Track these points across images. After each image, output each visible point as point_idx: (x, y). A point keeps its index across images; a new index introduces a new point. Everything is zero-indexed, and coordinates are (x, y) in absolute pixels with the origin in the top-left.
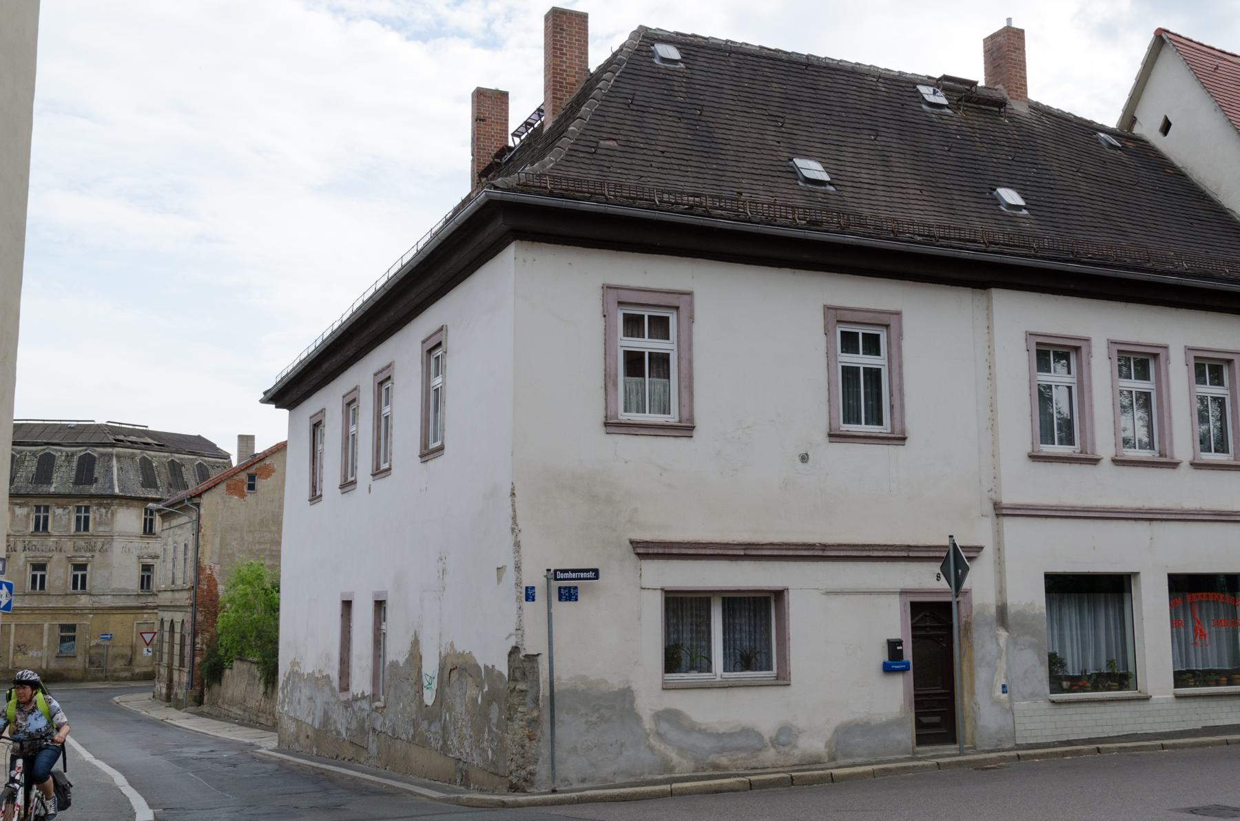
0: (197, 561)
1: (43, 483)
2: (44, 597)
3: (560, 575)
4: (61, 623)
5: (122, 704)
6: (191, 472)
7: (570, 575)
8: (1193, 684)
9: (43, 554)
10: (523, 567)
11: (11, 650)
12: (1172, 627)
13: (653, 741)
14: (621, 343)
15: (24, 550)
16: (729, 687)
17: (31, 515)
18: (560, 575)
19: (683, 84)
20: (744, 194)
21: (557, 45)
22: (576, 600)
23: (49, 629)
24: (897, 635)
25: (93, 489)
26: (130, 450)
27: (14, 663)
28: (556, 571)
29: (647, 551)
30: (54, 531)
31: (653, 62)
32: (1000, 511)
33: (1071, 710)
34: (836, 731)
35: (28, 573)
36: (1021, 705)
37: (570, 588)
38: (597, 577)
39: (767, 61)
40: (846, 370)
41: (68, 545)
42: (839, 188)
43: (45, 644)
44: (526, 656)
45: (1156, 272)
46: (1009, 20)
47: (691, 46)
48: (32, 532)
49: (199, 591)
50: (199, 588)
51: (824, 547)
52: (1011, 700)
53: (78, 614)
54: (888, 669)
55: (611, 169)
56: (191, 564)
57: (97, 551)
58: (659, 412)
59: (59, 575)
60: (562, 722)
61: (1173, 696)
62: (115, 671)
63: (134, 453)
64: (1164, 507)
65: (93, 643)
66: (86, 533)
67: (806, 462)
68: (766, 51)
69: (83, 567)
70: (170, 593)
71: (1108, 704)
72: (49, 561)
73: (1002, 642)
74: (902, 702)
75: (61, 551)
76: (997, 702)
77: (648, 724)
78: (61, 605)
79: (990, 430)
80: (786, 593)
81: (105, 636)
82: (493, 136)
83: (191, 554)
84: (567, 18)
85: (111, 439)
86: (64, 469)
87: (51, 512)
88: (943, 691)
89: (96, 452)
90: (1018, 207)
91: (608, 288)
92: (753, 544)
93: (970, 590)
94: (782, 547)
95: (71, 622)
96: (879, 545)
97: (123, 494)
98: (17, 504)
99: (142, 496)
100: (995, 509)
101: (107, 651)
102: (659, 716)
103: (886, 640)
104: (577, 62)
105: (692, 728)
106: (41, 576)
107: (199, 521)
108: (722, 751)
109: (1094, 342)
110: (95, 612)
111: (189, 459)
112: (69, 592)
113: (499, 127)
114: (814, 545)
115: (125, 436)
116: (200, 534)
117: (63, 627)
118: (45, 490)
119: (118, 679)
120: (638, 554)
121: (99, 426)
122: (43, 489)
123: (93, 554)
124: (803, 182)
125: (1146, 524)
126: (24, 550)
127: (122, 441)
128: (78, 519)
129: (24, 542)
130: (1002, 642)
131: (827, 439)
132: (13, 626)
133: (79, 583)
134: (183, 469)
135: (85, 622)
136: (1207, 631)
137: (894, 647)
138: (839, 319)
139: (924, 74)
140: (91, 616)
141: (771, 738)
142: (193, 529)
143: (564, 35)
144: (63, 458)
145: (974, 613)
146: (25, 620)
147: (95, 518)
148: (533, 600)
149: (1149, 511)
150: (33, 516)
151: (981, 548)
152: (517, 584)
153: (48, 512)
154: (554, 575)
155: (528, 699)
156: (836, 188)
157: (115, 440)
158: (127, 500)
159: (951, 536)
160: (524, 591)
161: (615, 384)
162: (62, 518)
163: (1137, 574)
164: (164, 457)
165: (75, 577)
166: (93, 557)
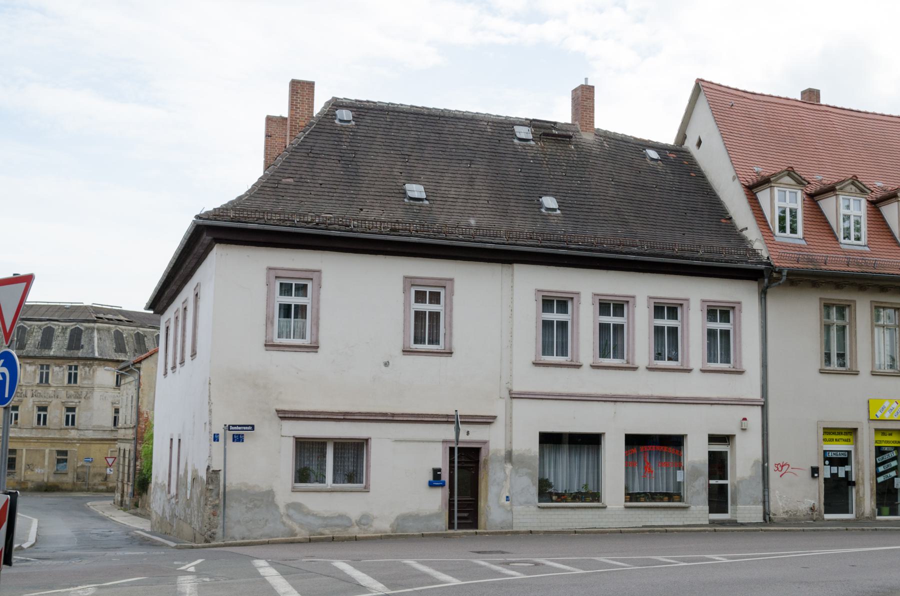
0: (138, 408)
1: (45, 348)
2: (45, 430)
3: (231, 428)
4: (57, 449)
5: (91, 507)
6: (152, 341)
7: (238, 428)
9: (45, 399)
10: (213, 423)
11: (23, 468)
12: (626, 466)
13: (285, 519)
14: (277, 299)
15: (32, 396)
17: (37, 371)
18: (231, 428)
19: (350, 136)
22: (243, 441)
23: (49, 454)
24: (438, 465)
25: (80, 353)
27: (25, 477)
28: (229, 426)
29: (285, 416)
31: (334, 123)
32: (514, 396)
33: (551, 512)
34: (397, 518)
36: (517, 508)
37: (239, 435)
38: (253, 429)
39: (413, 116)
41: (63, 393)
42: (432, 202)
43: (46, 463)
44: (213, 471)
45: (621, 253)
46: (586, 79)
47: (361, 109)
49: (139, 429)
50: (139, 427)
51: (393, 415)
52: (511, 505)
53: (69, 443)
54: (431, 485)
55: (309, 193)
56: (134, 410)
57: (83, 399)
58: (300, 338)
59: (56, 415)
60: (232, 507)
62: (94, 485)
65: (80, 464)
66: (75, 385)
68: (415, 108)
70: (124, 430)
71: (577, 510)
72: (49, 405)
73: (508, 471)
75: (57, 397)
76: (502, 506)
77: (282, 510)
78: (58, 437)
80: (369, 440)
82: (276, 146)
83: (134, 403)
84: (301, 86)
85: (94, 317)
86: (60, 338)
87: (51, 370)
88: (471, 499)
90: (554, 210)
92: (348, 413)
93: (489, 441)
95: (64, 449)
96: (428, 415)
98: (27, 363)
100: (510, 394)
101: (89, 470)
102: (289, 506)
104: (306, 112)
105: (308, 513)
108: (326, 526)
109: (582, 296)
110: (81, 442)
111: (150, 331)
112: (63, 427)
113: (281, 141)
114: (387, 414)
115: (104, 314)
116: (140, 389)
117: (59, 453)
118: (47, 353)
119: (97, 491)
120: (280, 417)
121: (86, 307)
122: (46, 353)
123: (80, 400)
124: (408, 199)
125: (613, 403)
126: (32, 396)
127: (101, 318)
128: (70, 374)
129: (32, 390)
130: (508, 471)
131: (402, 353)
132: (24, 451)
133: (70, 421)
134: (146, 339)
135: (74, 449)
136: (653, 469)
137: (436, 473)
140: (78, 445)
141: (356, 521)
142: (135, 386)
143: (299, 96)
144: (60, 330)
145: (490, 454)
146: (33, 446)
147: (81, 374)
148: (218, 441)
150: (38, 372)
151: (495, 417)
152: (209, 432)
153: (49, 369)
154: (229, 428)
155: (213, 494)
157: (97, 318)
159: (456, 411)
160: (213, 436)
161: (272, 323)
163: (686, 435)
164: (132, 330)
165: (68, 417)
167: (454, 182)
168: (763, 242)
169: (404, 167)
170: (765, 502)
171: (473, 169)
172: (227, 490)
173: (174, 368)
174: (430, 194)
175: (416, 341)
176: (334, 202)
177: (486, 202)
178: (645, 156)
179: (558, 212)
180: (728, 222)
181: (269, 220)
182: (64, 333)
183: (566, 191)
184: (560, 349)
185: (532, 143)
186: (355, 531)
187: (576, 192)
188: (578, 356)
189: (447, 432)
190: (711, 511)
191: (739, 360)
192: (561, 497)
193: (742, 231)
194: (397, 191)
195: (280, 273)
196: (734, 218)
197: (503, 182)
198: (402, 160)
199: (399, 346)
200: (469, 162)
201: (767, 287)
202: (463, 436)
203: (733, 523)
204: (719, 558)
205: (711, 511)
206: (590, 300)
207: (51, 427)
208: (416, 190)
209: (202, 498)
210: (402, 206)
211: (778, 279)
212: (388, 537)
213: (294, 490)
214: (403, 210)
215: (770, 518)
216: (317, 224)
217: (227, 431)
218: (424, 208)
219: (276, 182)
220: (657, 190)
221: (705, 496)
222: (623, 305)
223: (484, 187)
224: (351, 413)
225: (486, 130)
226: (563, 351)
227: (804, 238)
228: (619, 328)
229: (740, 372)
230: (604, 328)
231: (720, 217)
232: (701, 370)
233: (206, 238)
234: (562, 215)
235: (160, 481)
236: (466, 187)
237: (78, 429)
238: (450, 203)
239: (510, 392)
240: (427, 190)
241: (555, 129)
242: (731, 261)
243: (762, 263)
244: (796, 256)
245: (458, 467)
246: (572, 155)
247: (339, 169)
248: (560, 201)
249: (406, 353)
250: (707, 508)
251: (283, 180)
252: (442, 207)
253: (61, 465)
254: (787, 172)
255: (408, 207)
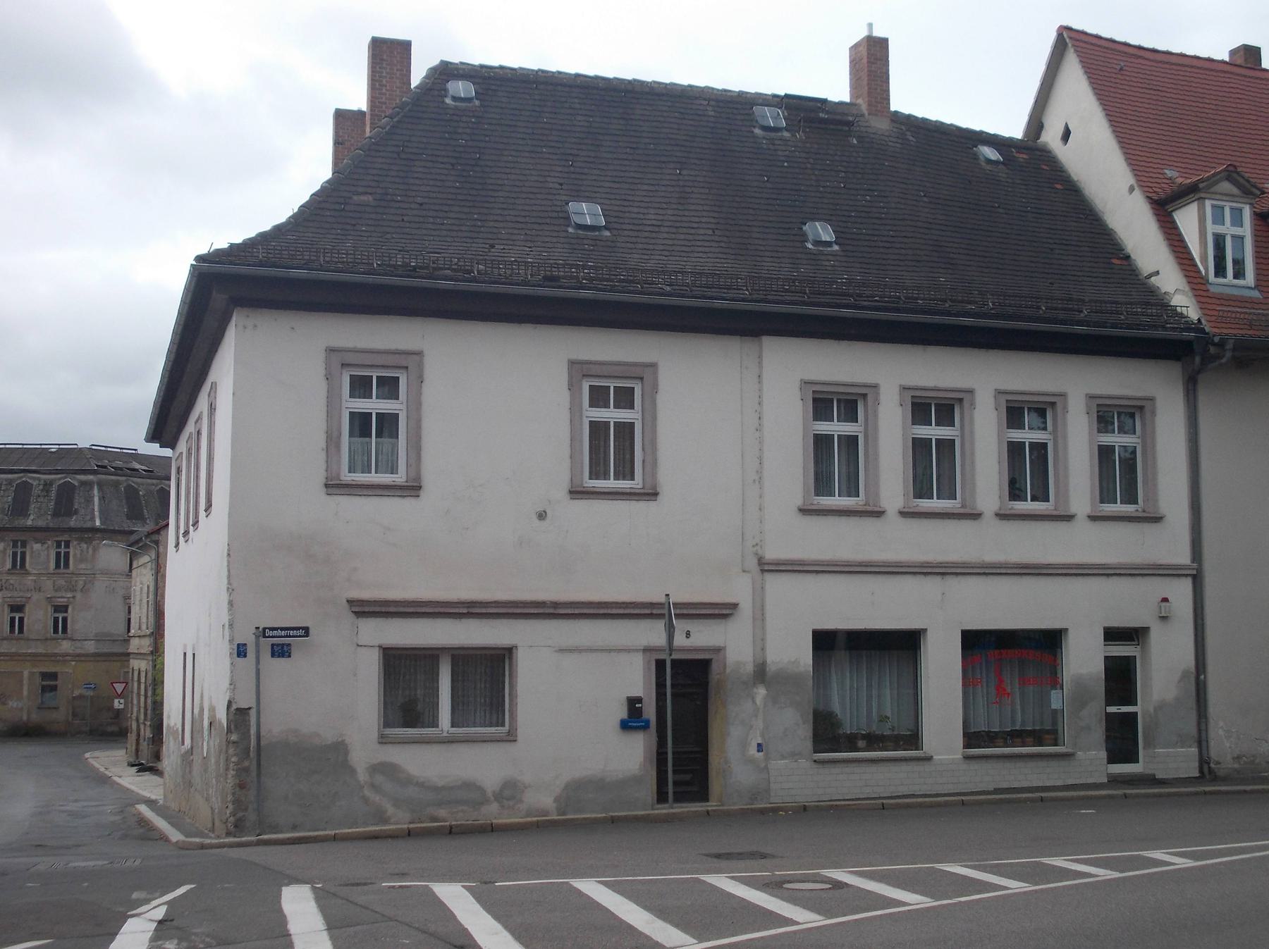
2: (23, 642)
3: (268, 633)
5: (90, 760)
8: (1001, 744)
9: (21, 594)
12: (964, 685)
14: (345, 404)
16: (448, 742)
17: (8, 551)
18: (268, 633)
20: (497, 246)
21: (375, 76)
22: (290, 656)
24: (637, 692)
25: (73, 522)
26: (113, 477)
28: (264, 629)
29: (365, 609)
30: (33, 568)
31: (443, 102)
32: (768, 567)
33: (836, 770)
34: (567, 786)
35: (6, 617)
36: (778, 764)
37: (283, 645)
38: (307, 634)
40: (593, 425)
42: (615, 232)
43: (25, 693)
45: (949, 314)
46: (870, 26)
48: (9, 570)
51: (556, 605)
52: (767, 758)
53: (58, 661)
55: (400, 218)
61: (961, 757)
63: (118, 480)
64: (960, 560)
65: (76, 693)
67: (540, 520)
69: (65, 609)
70: (137, 638)
73: (759, 700)
74: (642, 760)
75: (40, 591)
76: (751, 761)
77: (362, 776)
79: (757, 482)
80: (514, 651)
81: (88, 686)
89: (75, 480)
90: (829, 244)
91: (331, 351)
94: (508, 605)
95: (52, 669)
96: (617, 603)
97: (105, 527)
99: (126, 529)
102: (376, 769)
103: (625, 699)
105: (408, 781)
106: (19, 618)
107: (158, 560)
110: (77, 658)
112: (49, 636)
117: (45, 676)
120: (355, 613)
125: (938, 578)
128: (58, 554)
131: (568, 496)
133: (61, 627)
137: (634, 705)
138: (585, 373)
139: (769, 93)
140: (73, 663)
143: (384, 65)
144: (41, 487)
145: (728, 671)
148: (245, 656)
149: (940, 565)
150: (10, 552)
151: (735, 606)
153: (25, 547)
154: (263, 633)
156: (611, 233)
158: (108, 533)
159: (667, 595)
162: (41, 554)
166: (74, 597)
167: (652, 199)
168: (1190, 294)
169: (566, 175)
170: (1202, 741)
171: (686, 178)
172: (262, 743)
173: (186, 533)
174: (613, 220)
175: (594, 475)
176: (445, 233)
177: (710, 232)
178: (976, 157)
179: (836, 247)
180: (1125, 262)
181: (328, 262)
182: (47, 492)
183: (846, 213)
184: (844, 488)
185: (786, 134)
186: (492, 813)
187: (863, 214)
188: (877, 495)
189: (653, 633)
190: (1112, 760)
191: (1152, 496)
192: (851, 743)
193: (1150, 276)
194: (555, 215)
195: (351, 358)
196: (1133, 256)
197: (737, 199)
198: (563, 163)
199: (565, 485)
200: (678, 166)
201: (1199, 372)
202: (679, 640)
203: (1150, 780)
204: (1173, 859)
205: (1112, 760)
206: (896, 398)
207: (32, 637)
208: (587, 212)
209: (221, 757)
210: (562, 240)
211: (1218, 357)
212: (553, 824)
213: (383, 740)
214: (566, 246)
215: (1209, 767)
216: (415, 268)
217: (262, 639)
218: (602, 243)
219: (342, 200)
220: (1001, 210)
221: (1099, 733)
222: (953, 406)
223: (705, 208)
224: (481, 603)
225: (706, 112)
226: (852, 488)
227: (1257, 287)
228: (946, 446)
229: (1156, 518)
230: (920, 446)
231: (1110, 256)
232: (1089, 517)
233: (219, 299)
234: (842, 254)
235: (172, 724)
236: (675, 206)
237: (72, 639)
238: (646, 234)
239: (761, 562)
240: (607, 213)
241: (823, 111)
242: (1138, 326)
243: (1189, 329)
244: (1246, 316)
245: (673, 695)
246: (854, 154)
247: (452, 178)
248: (839, 229)
249: (576, 496)
250: (1103, 755)
251: (355, 198)
252: (634, 240)
253: (48, 695)
254: (1226, 173)
255: (574, 241)
